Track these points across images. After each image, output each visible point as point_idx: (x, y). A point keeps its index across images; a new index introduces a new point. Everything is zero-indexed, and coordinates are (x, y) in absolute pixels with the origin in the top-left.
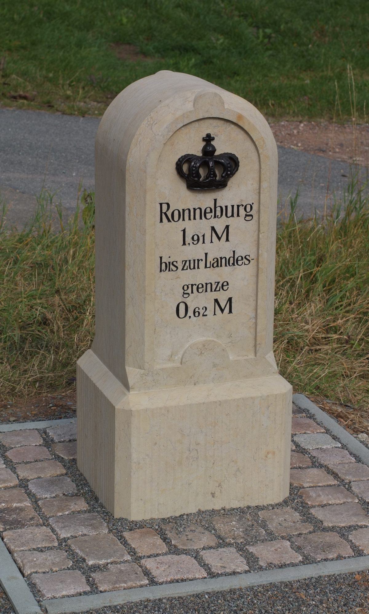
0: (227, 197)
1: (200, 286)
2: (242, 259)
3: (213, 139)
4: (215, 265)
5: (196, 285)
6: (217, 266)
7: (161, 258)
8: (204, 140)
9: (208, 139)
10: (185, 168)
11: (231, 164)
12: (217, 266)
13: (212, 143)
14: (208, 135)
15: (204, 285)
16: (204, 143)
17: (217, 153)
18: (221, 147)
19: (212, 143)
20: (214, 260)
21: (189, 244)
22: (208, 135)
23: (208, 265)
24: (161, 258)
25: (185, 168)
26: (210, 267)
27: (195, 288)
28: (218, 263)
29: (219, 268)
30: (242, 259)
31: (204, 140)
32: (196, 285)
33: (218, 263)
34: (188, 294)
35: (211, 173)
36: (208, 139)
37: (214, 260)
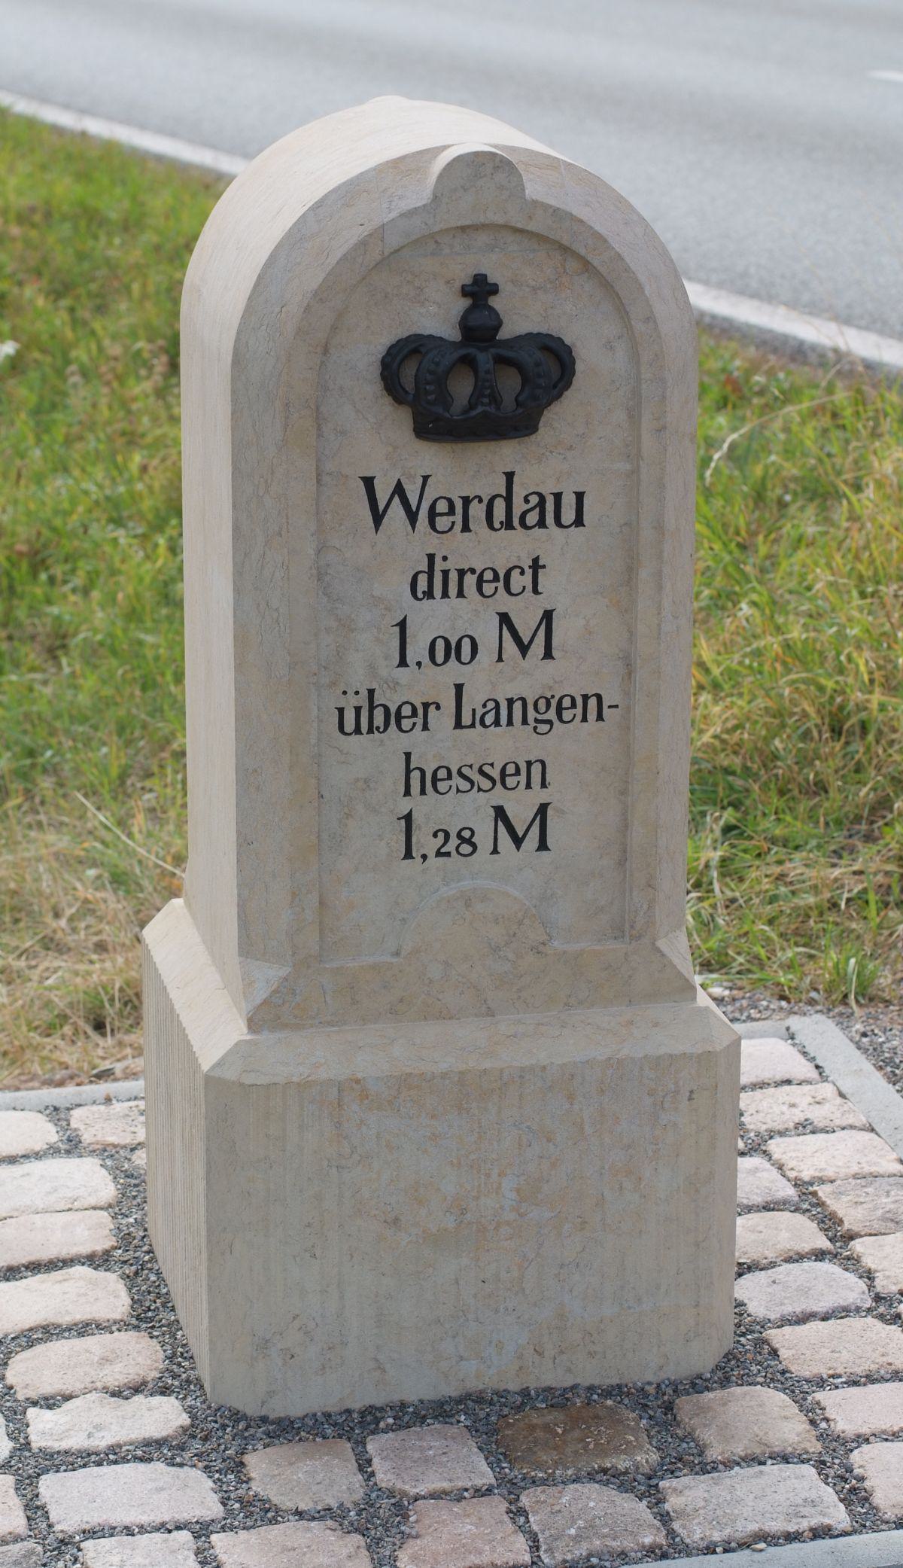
0: (538, 464)
1: (567, 703)
2: (450, 777)
3: (494, 290)
4: (489, 719)
5: (473, 571)
6: (497, 723)
7: (408, 755)
8: (465, 292)
9: (480, 290)
10: (408, 373)
11: (550, 367)
12: (497, 723)
13: (495, 302)
14: (480, 280)
15: (579, 702)
16: (465, 303)
17: (504, 334)
18: (520, 315)
19: (495, 302)
20: (484, 706)
21: (419, 664)
22: (480, 280)
23: (466, 719)
24: (408, 755)
25: (408, 373)
26: (473, 725)
27: (470, 580)
28: (501, 713)
29: (503, 729)
30: (450, 777)
31: (465, 292)
32: (473, 571)
33: (501, 713)
34: (550, 722)
35: (484, 391)
36: (480, 290)
37: (484, 706)
